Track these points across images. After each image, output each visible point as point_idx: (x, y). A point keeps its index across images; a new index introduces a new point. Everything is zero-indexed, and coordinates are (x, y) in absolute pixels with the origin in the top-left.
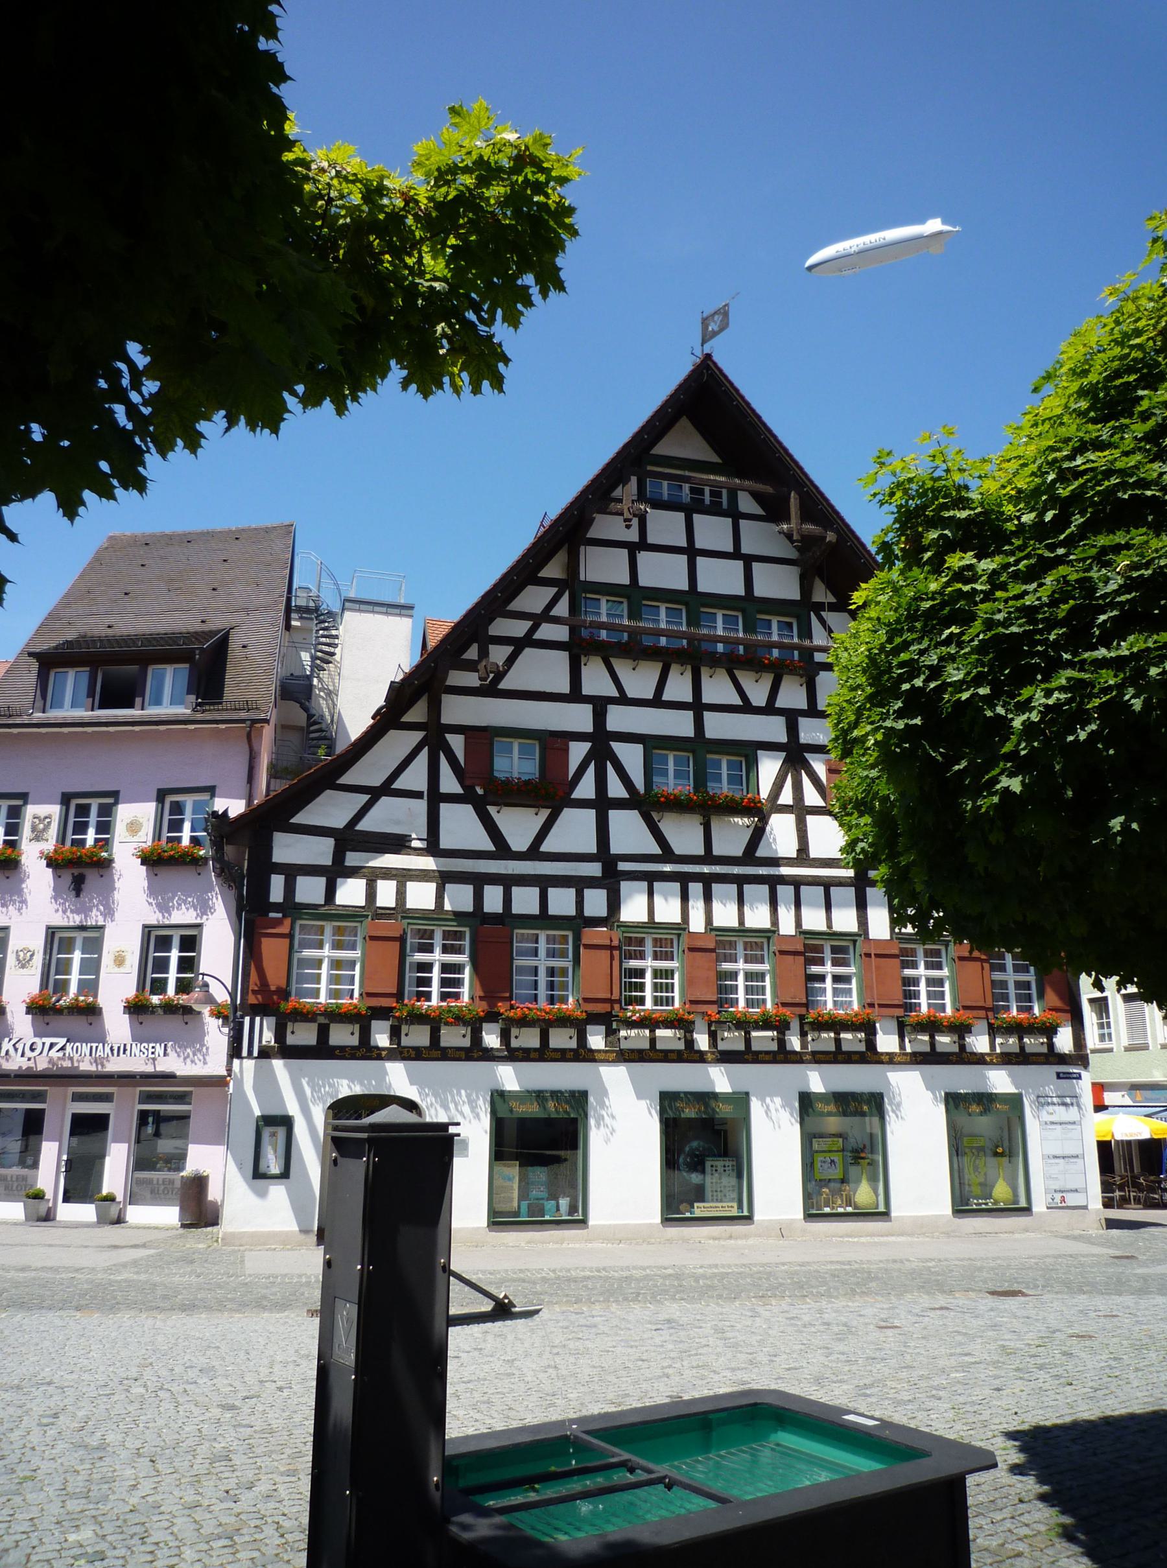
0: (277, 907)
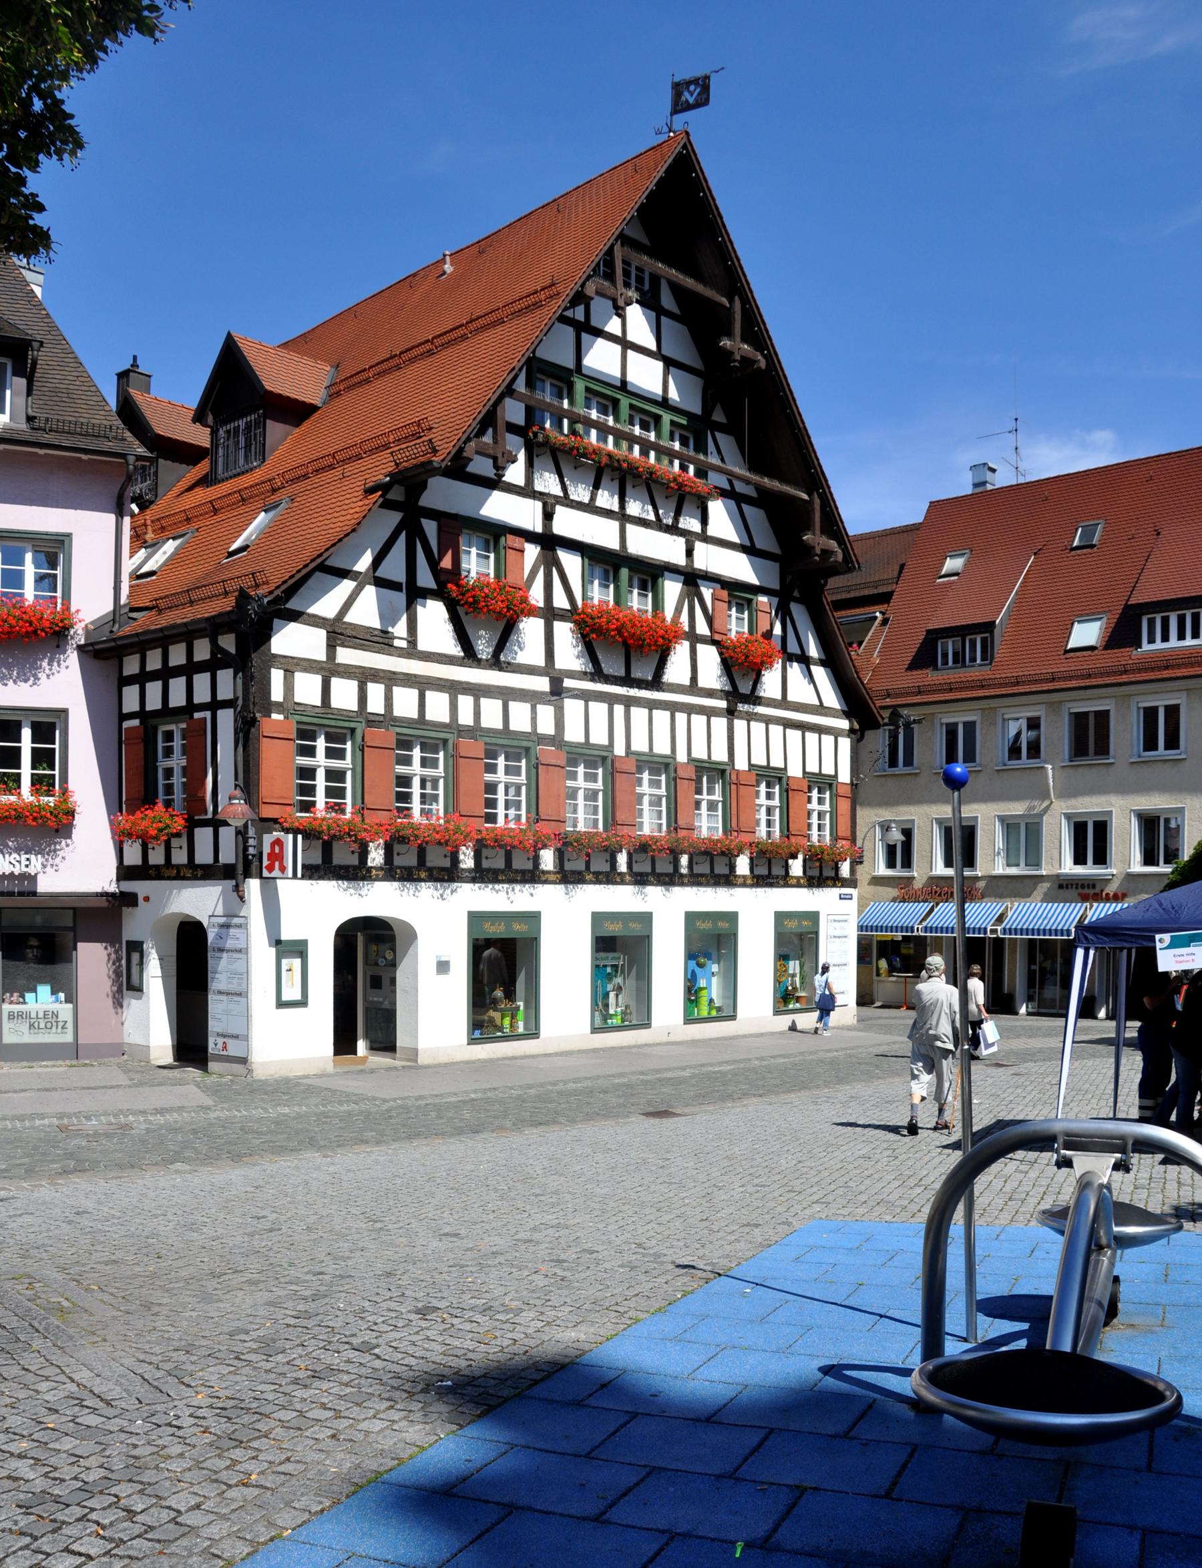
0: (279, 707)
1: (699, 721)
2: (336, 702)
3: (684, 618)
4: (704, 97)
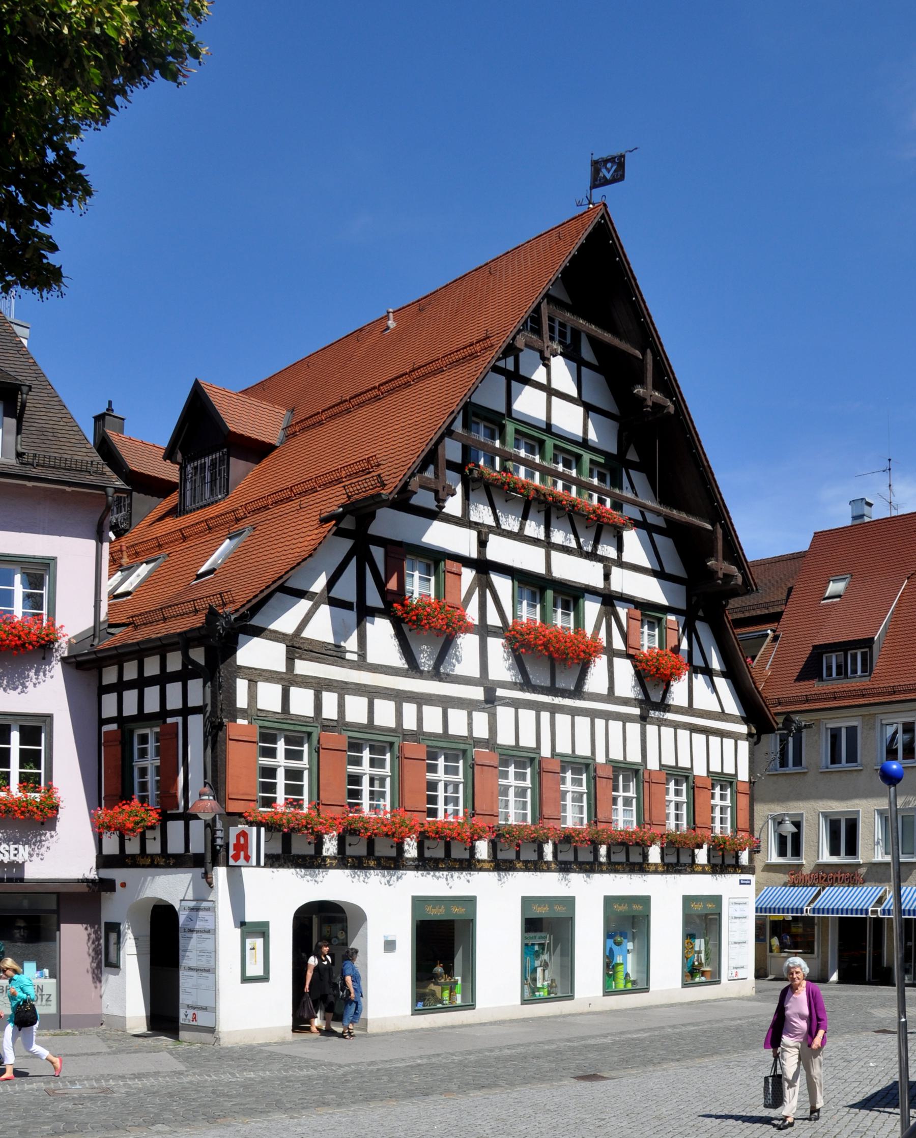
0: (244, 713)
1: (615, 726)
2: (294, 709)
4: (620, 173)
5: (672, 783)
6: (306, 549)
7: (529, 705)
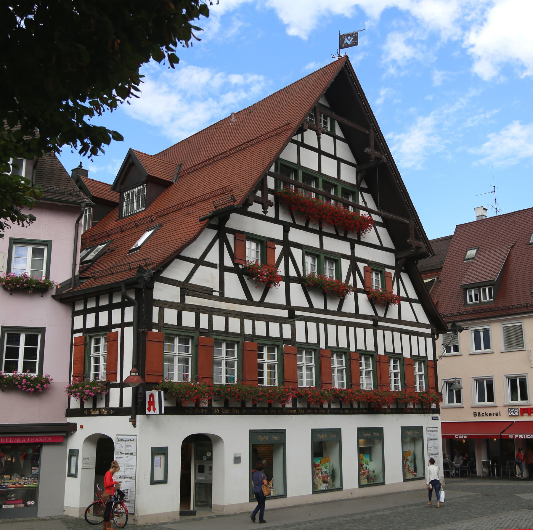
0: (156, 326)
1: (360, 331)
2: (185, 323)
3: (351, 282)
4: (355, 41)
5: (363, 359)
6: (192, 235)
7: (312, 319)
